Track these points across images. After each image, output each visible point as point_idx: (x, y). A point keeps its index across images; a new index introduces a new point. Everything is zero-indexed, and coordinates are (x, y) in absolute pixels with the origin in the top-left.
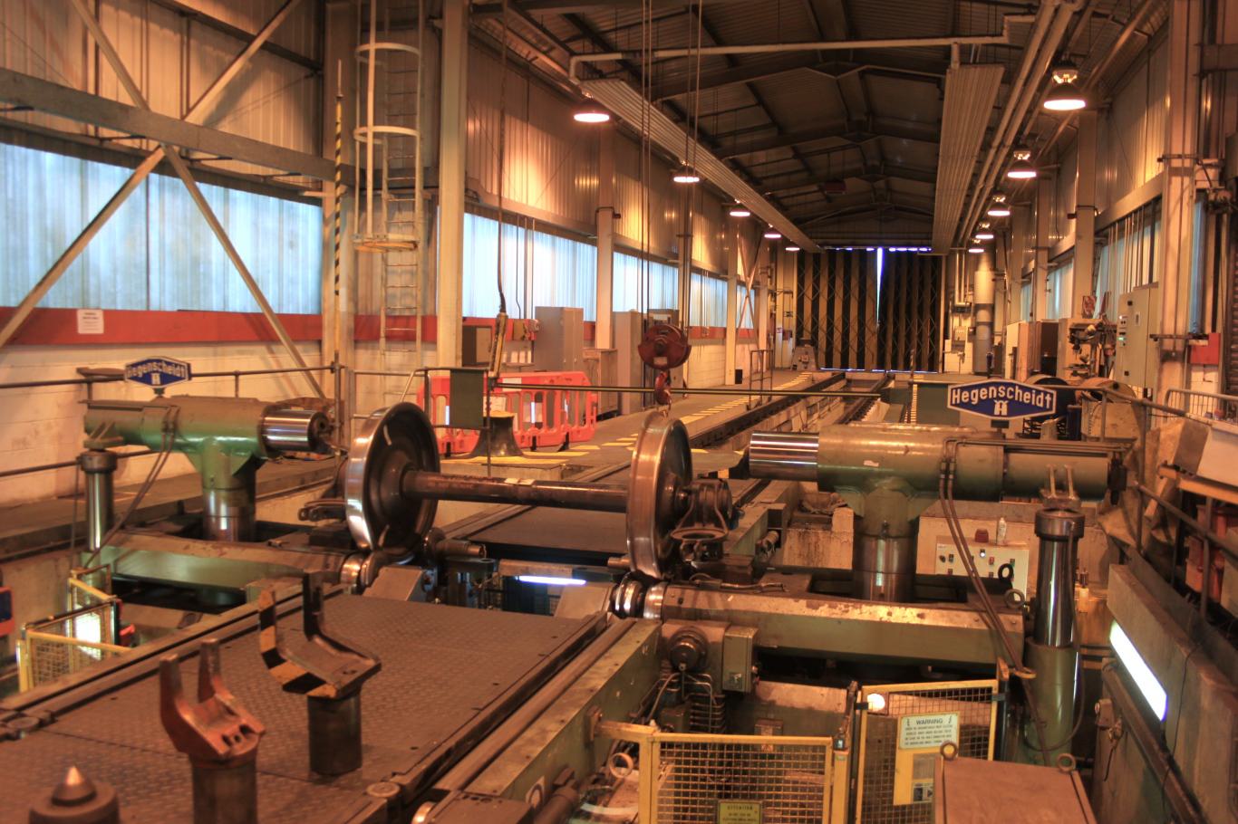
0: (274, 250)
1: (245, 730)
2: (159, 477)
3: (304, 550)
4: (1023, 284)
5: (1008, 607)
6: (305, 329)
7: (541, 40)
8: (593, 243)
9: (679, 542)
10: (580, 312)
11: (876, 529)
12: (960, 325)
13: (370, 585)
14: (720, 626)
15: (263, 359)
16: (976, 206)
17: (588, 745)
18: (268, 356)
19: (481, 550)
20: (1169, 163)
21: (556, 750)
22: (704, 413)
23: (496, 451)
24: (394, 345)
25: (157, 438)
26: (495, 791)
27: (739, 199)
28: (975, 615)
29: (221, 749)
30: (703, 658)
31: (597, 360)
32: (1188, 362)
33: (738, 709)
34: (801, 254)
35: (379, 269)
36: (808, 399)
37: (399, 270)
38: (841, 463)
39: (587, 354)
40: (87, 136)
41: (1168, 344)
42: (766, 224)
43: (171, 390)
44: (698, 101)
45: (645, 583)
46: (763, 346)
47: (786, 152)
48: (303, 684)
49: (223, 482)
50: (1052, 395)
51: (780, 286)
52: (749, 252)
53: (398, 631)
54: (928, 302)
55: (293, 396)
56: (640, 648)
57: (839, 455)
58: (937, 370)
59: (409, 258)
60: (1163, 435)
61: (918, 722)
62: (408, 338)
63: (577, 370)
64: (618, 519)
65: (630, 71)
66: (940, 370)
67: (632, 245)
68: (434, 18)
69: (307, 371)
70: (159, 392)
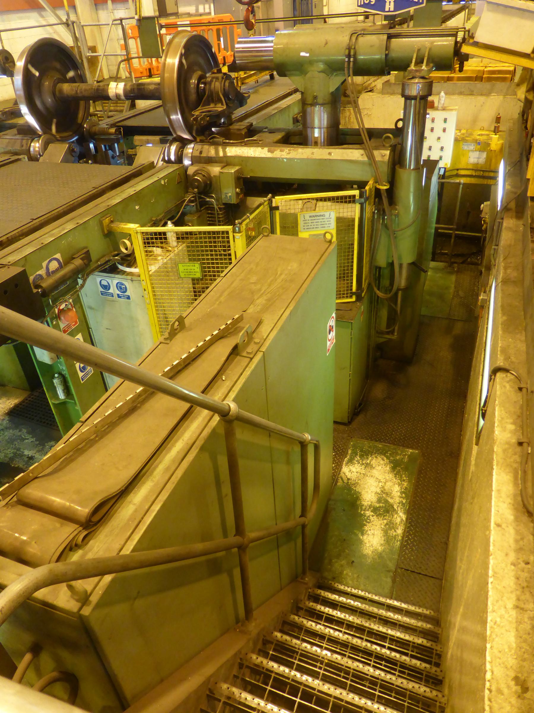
5: (384, 146)
30: (208, 187)
45: (184, 143)
61: (310, 217)
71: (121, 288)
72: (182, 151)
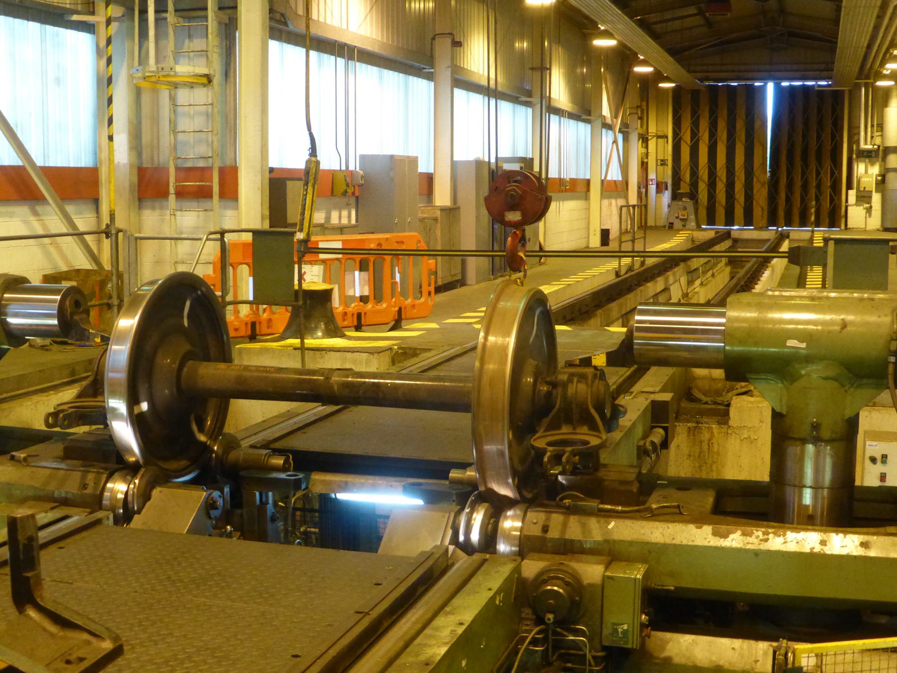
3: (55, 465)
6: (77, 185)
8: (430, 77)
9: (544, 452)
10: (413, 161)
11: (804, 430)
12: (866, 172)
13: (139, 512)
14: (598, 563)
15: (25, 222)
18: (32, 219)
22: (566, 281)
23: (311, 332)
24: (186, 204)
27: (604, 23)
30: (578, 605)
31: (436, 220)
34: (677, 91)
36: (689, 263)
37: (192, 110)
38: (756, 344)
39: (423, 211)
42: (636, 54)
45: (498, 506)
46: (633, 199)
51: (652, 129)
54: (828, 147)
55: (64, 268)
56: (493, 599)
57: (752, 333)
58: (839, 227)
59: (201, 95)
62: (204, 194)
63: (410, 231)
64: (463, 419)
66: (843, 227)
67: (475, 80)
69: (80, 235)
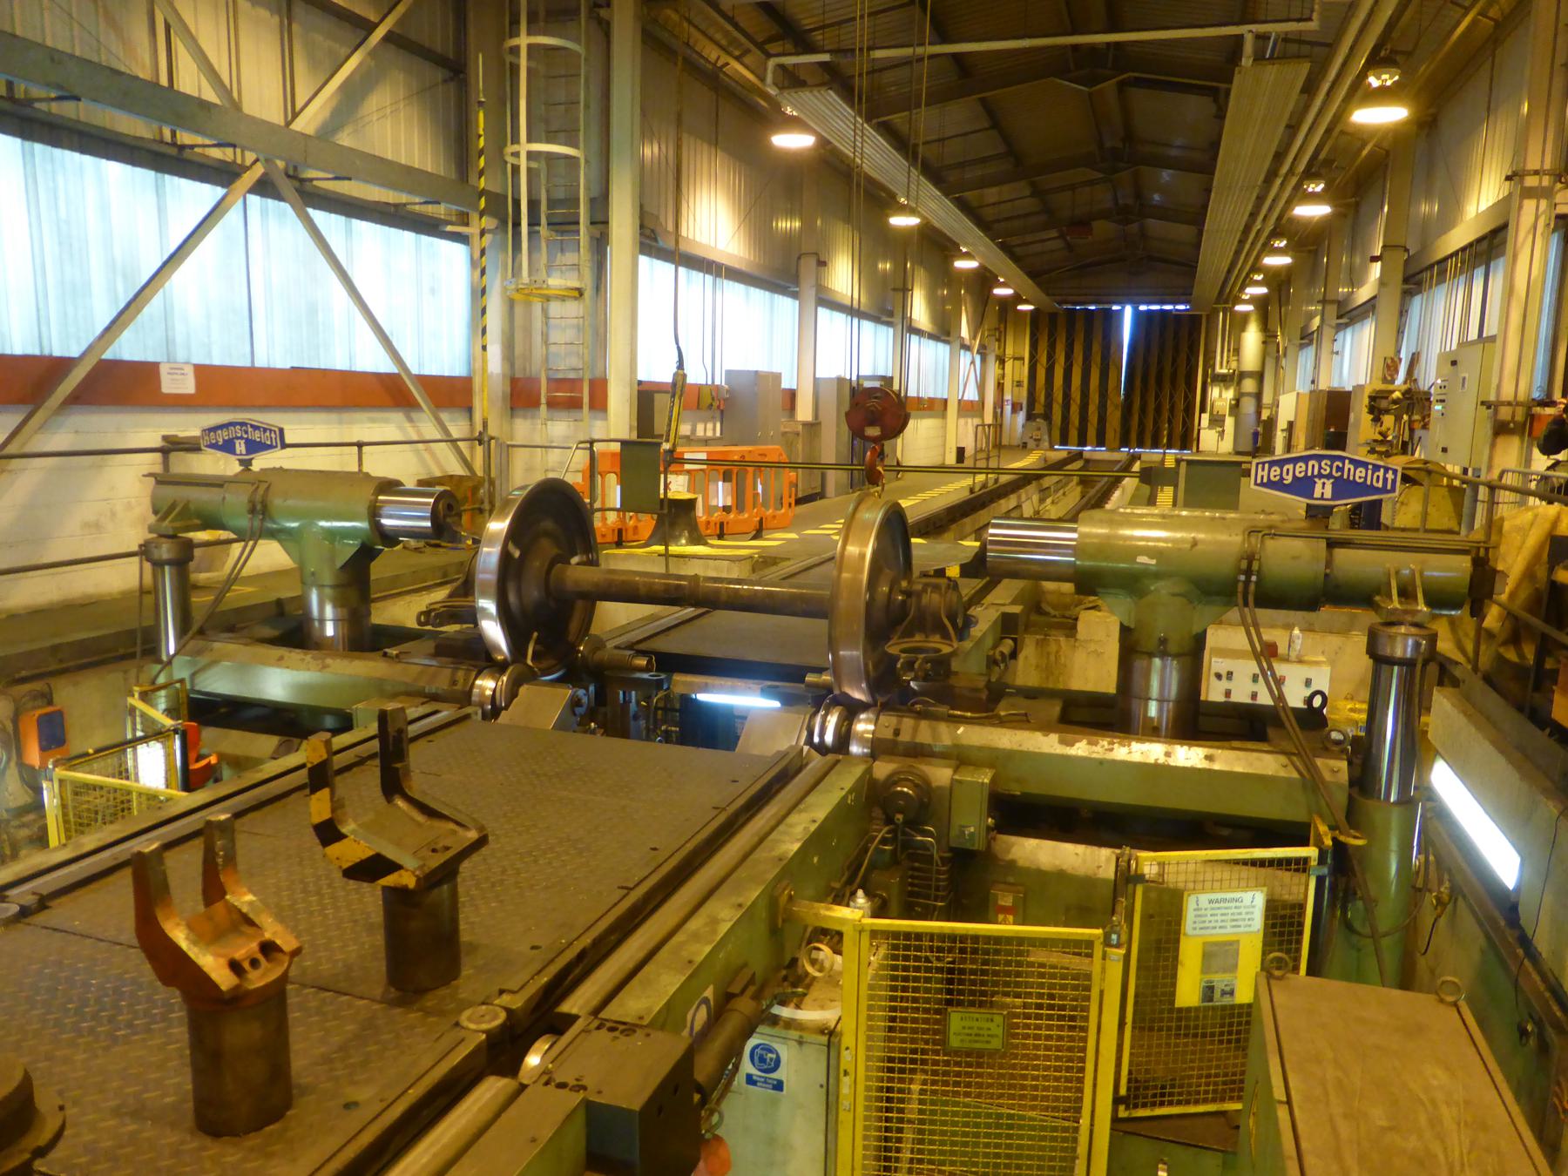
0: (416, 298)
1: (268, 948)
2: (244, 573)
3: (427, 662)
4: (1302, 347)
5: (1326, 749)
6: (450, 394)
7: (734, 42)
13: (506, 708)
15: (401, 428)
16: (1248, 255)
17: (775, 931)
18: (407, 425)
19: (649, 662)
20: (1522, 181)
21: (730, 946)
22: (922, 496)
23: (675, 539)
24: (557, 414)
25: (243, 522)
26: (641, 1018)
27: (965, 245)
28: (1283, 759)
29: (223, 978)
30: (926, 807)
32: (1530, 434)
33: (966, 881)
34: (1034, 315)
35: (538, 323)
38: (1106, 559)
39: (785, 426)
40: (162, 141)
41: (1505, 413)
43: (261, 462)
44: (925, 122)
45: (852, 710)
46: (989, 419)
47: (1021, 188)
48: (372, 868)
49: (328, 578)
50: (1395, 472)
51: (1009, 351)
52: (975, 311)
53: (533, 772)
55: (438, 474)
56: (845, 798)
57: (1104, 548)
59: (572, 309)
60: (1507, 526)
61: (1211, 902)
62: (573, 404)
65: (836, 78)
67: (839, 299)
68: (600, 6)
69: (453, 441)
70: (246, 464)
71: (762, 1060)
72: (850, 725)
